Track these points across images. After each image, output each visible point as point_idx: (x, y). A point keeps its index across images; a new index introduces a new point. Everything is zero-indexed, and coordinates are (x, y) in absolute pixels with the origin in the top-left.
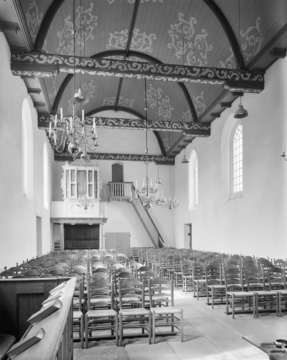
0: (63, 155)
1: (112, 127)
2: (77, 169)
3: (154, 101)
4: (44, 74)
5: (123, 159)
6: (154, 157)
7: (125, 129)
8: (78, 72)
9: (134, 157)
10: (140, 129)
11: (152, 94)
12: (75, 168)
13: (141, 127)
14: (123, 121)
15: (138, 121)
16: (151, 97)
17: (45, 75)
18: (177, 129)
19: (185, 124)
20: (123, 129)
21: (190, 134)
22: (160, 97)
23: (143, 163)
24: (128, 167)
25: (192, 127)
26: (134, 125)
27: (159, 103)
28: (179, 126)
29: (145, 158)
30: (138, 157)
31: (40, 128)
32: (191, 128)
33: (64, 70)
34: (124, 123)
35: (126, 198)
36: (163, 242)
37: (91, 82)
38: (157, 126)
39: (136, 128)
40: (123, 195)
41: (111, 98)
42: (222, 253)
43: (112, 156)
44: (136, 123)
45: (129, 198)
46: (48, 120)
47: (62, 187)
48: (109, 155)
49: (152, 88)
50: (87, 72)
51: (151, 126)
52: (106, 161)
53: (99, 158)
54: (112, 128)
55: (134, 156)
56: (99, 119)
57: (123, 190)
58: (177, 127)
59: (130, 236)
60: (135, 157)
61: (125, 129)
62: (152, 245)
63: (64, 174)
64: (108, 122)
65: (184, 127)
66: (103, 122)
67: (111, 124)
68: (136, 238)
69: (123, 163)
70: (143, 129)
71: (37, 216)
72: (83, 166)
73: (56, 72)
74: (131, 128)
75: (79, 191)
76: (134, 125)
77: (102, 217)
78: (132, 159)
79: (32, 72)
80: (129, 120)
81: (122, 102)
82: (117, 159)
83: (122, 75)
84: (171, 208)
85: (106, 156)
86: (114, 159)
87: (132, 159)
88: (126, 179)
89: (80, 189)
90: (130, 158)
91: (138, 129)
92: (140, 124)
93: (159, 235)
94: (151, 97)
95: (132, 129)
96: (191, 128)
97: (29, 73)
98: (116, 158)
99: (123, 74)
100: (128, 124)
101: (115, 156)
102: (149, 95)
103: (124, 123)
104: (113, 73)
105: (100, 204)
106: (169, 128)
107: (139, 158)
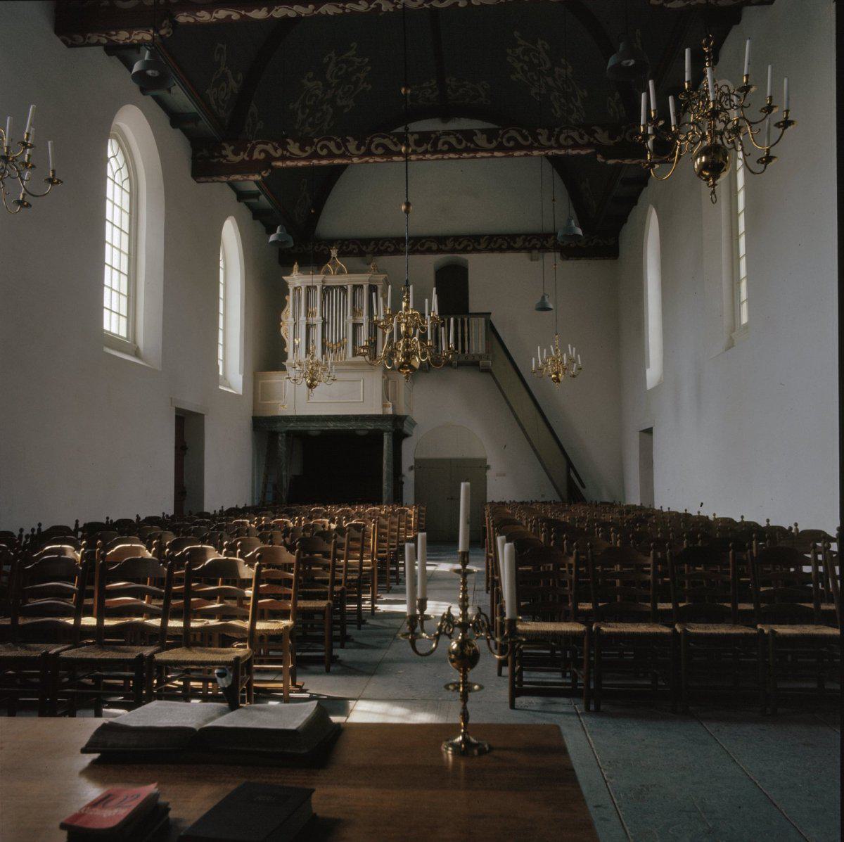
0: (299, 250)
1: (385, 160)
2: (323, 281)
3: (535, 78)
4: (136, 32)
5: (465, 251)
6: (524, 237)
7: (421, 160)
8: (223, 17)
9: (495, 242)
10: (465, 155)
11: (526, 58)
12: (317, 280)
13: (467, 150)
14: (415, 140)
15: (458, 135)
16: (526, 68)
17: (139, 37)
18: (576, 146)
19: (599, 130)
20: (418, 160)
21: (617, 158)
22: (549, 65)
23: (522, 257)
24: (480, 266)
25: (622, 136)
26: (446, 147)
27: (550, 80)
28: (581, 136)
29: (527, 243)
30: (506, 241)
31: (198, 180)
32: (618, 139)
33: (187, 16)
34: (418, 143)
35: (470, 359)
36: (584, 486)
37: (352, 48)
38: (512, 144)
39: (452, 155)
40: (466, 348)
41: (424, 85)
42: (721, 516)
43: (431, 242)
44: (453, 141)
45: (477, 358)
46: (217, 157)
47: (283, 334)
48: (424, 241)
49: (521, 42)
50: (243, 12)
51: (494, 144)
52: (417, 258)
53: (398, 252)
54: (387, 161)
55: (495, 239)
56: (349, 141)
57: (466, 335)
58: (573, 139)
59: (488, 467)
60: (500, 241)
61: (421, 160)
62: (558, 499)
63: (290, 299)
64: (373, 147)
65: (595, 139)
66: (358, 148)
67: (380, 151)
68: (504, 475)
69: (467, 261)
70: (471, 155)
71: (176, 408)
72: (338, 274)
73: (163, 25)
74: (440, 156)
75: (327, 343)
76: (446, 147)
77: (390, 411)
78: (489, 247)
79: (107, 34)
80: (433, 136)
81: (458, 94)
82: (446, 249)
83: (338, 7)
84: (558, 381)
85: (420, 244)
86: (439, 251)
87: (489, 247)
88: (473, 308)
89: (329, 335)
90: (483, 246)
91: (459, 158)
92: (464, 142)
93: (570, 465)
94: (526, 68)
95: (443, 159)
96: (618, 139)
97: (99, 36)
98: (443, 247)
99: (341, 5)
100: (430, 145)
101: (437, 243)
102: (521, 64)
103: (418, 143)
104: (311, 7)
105: (383, 377)
106: (551, 147)
107: (512, 244)
